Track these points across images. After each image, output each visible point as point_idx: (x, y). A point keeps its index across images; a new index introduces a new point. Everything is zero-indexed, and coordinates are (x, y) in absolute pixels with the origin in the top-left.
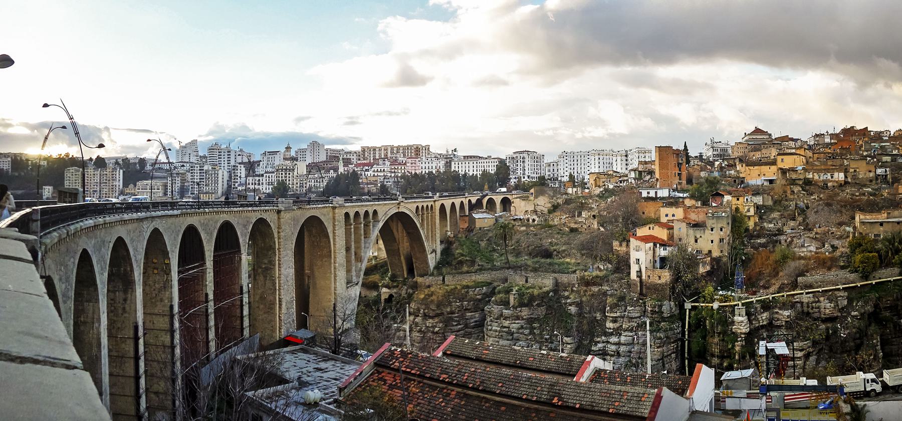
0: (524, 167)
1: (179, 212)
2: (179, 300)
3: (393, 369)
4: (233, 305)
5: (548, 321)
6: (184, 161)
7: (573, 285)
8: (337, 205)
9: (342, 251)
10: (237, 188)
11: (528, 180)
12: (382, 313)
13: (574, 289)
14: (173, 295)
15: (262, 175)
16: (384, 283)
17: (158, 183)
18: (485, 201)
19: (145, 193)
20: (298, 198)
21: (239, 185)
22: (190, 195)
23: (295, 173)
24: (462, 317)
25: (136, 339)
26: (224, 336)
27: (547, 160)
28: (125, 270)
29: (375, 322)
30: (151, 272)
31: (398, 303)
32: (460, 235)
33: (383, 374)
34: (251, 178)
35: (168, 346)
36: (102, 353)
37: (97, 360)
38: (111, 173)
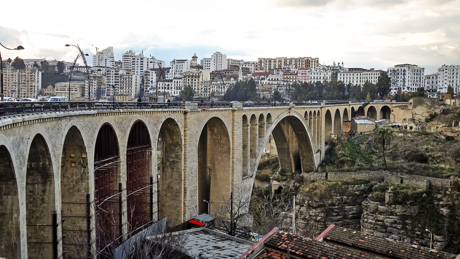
0: (404, 79)
1: (95, 112)
2: (95, 190)
3: (280, 250)
4: (144, 193)
5: (420, 219)
6: (100, 65)
7: (447, 189)
8: (236, 109)
9: (239, 148)
10: (149, 91)
11: (408, 91)
12: (272, 202)
13: (448, 192)
14: (90, 186)
15: (171, 81)
16: (275, 177)
17: (76, 85)
18: (366, 109)
19: (63, 94)
20: (202, 101)
21: (150, 89)
22: (105, 96)
23: (201, 80)
24: (342, 209)
25: (55, 226)
26: (135, 220)
27: (426, 73)
28: (44, 164)
29: (266, 209)
30: (69, 166)
31: (286, 194)
32: (343, 138)
33: (271, 253)
34: (161, 83)
35: (85, 231)
36: (21, 241)
37: (16, 248)
38: (29, 75)
